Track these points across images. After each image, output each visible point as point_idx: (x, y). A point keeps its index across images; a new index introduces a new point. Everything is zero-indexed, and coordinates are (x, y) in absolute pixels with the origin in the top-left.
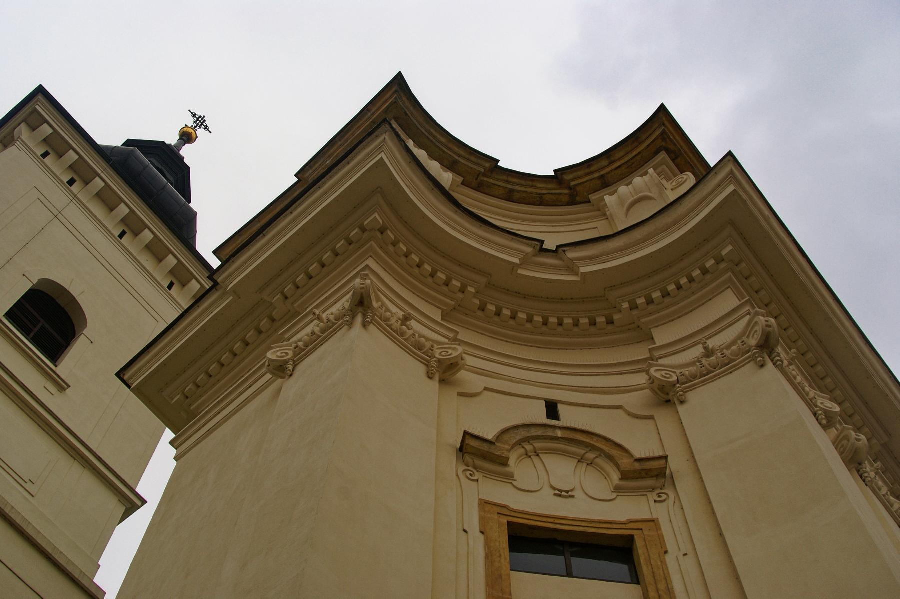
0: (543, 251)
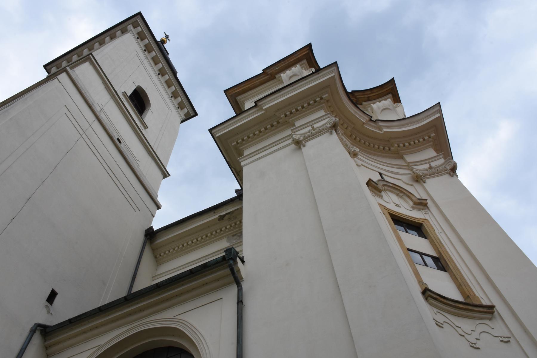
0: (371, 120)
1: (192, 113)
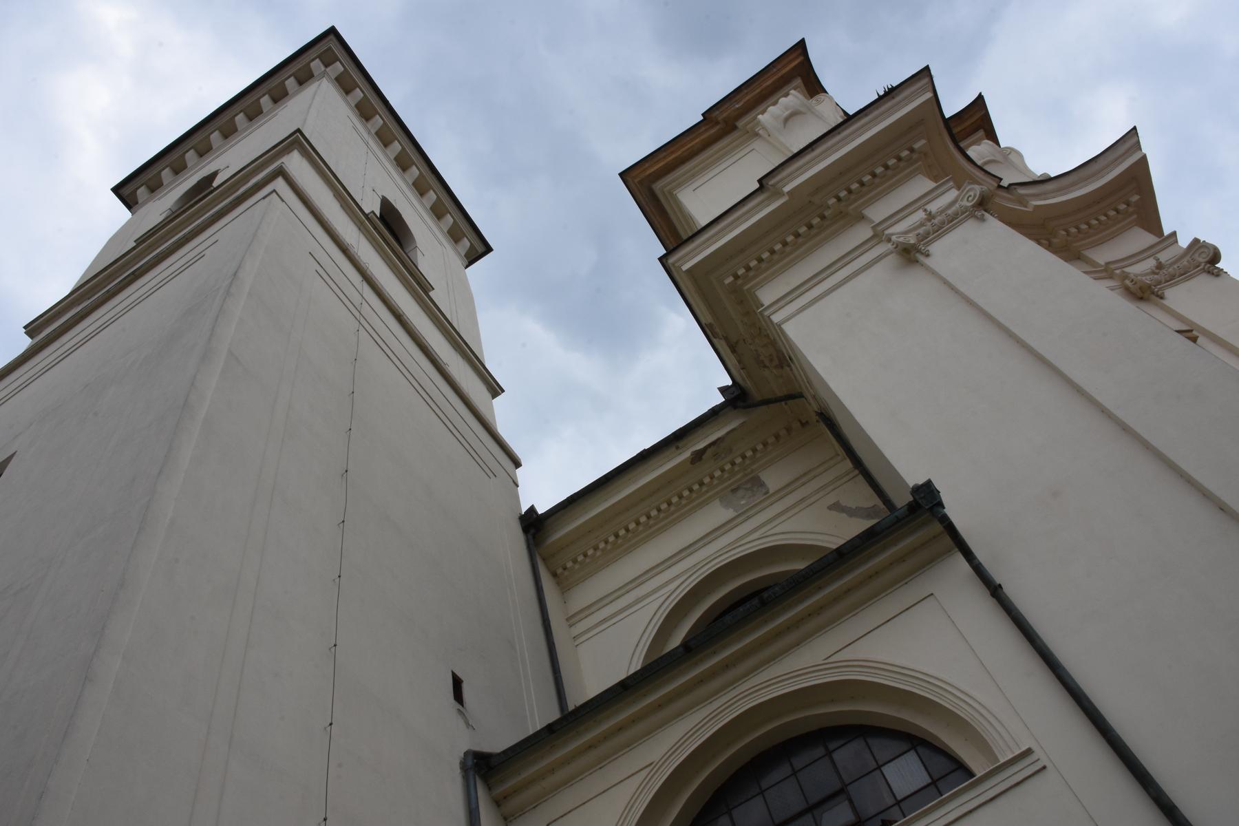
0: (1000, 187)
1: (481, 249)
